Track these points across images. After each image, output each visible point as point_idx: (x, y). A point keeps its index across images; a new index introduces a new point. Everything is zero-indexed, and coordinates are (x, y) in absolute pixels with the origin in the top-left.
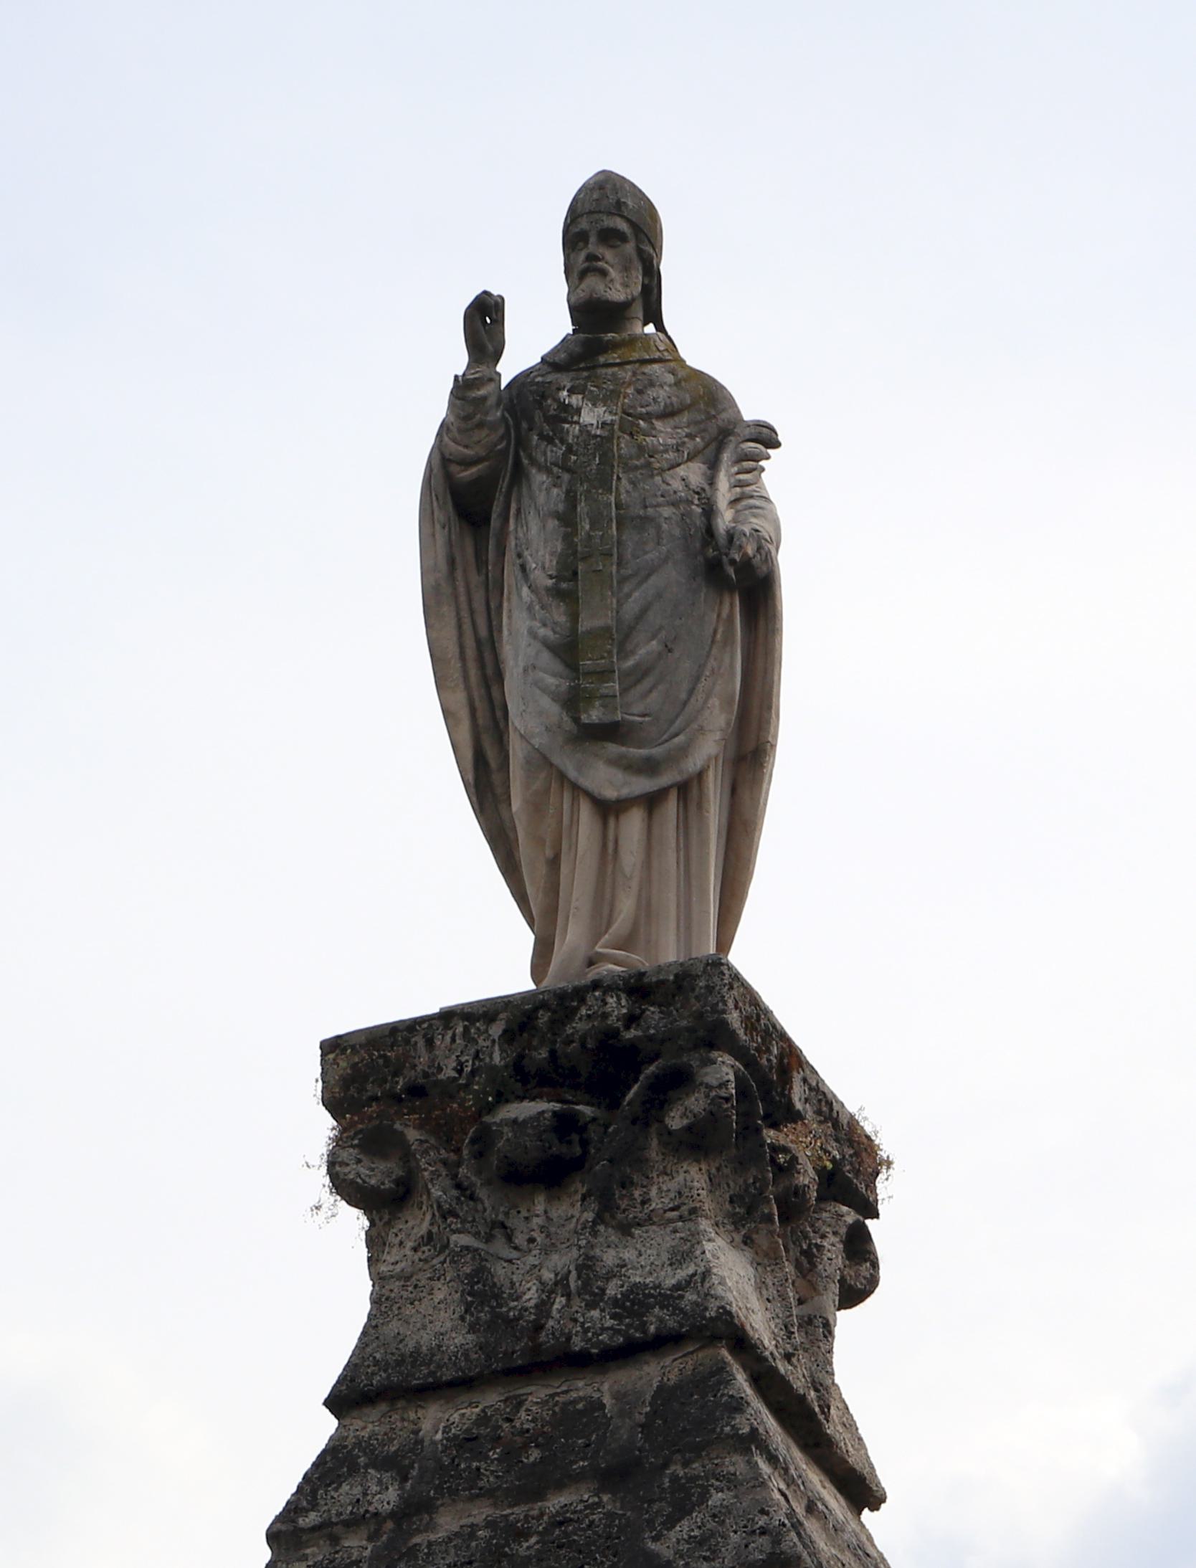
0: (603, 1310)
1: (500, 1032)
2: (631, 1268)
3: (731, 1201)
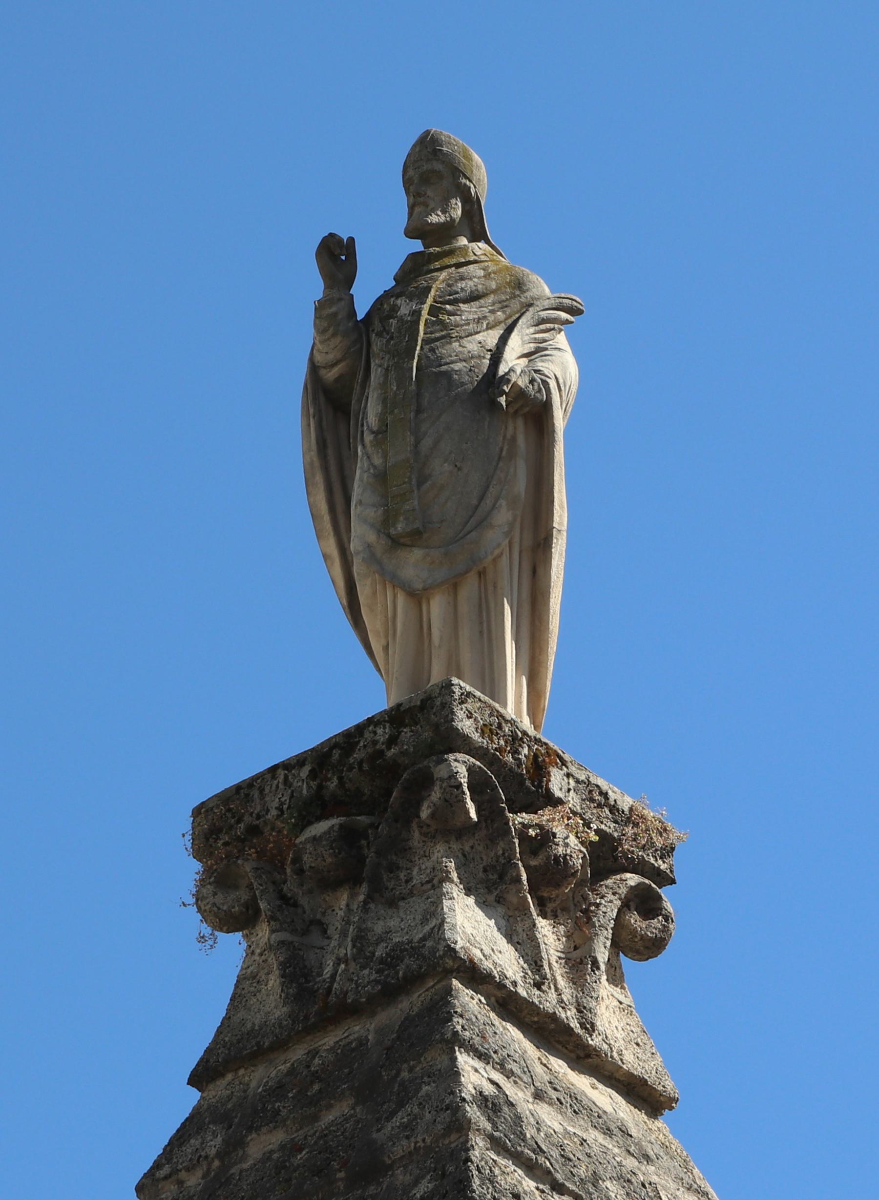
0: (371, 969)
1: (307, 773)
2: (395, 933)
3: (485, 870)
